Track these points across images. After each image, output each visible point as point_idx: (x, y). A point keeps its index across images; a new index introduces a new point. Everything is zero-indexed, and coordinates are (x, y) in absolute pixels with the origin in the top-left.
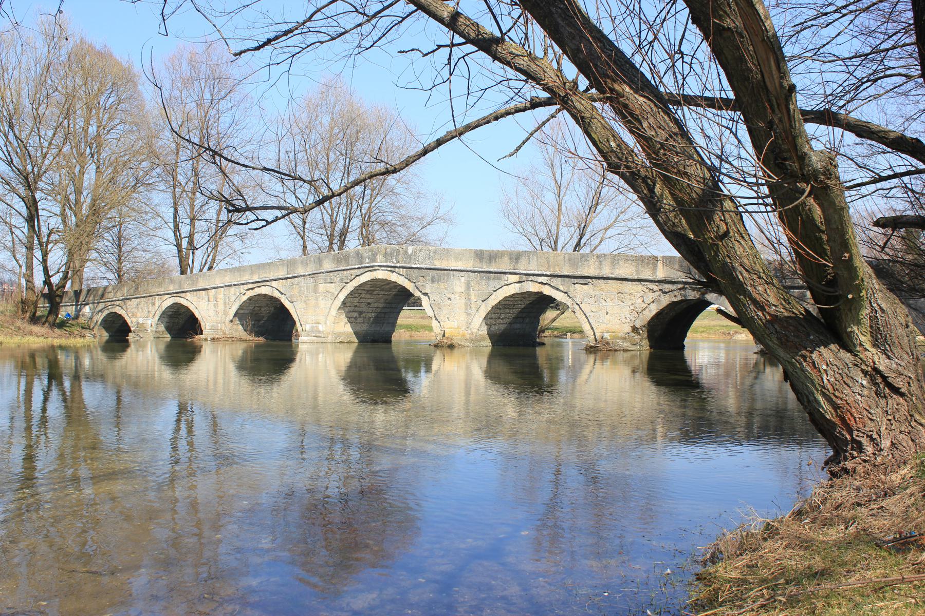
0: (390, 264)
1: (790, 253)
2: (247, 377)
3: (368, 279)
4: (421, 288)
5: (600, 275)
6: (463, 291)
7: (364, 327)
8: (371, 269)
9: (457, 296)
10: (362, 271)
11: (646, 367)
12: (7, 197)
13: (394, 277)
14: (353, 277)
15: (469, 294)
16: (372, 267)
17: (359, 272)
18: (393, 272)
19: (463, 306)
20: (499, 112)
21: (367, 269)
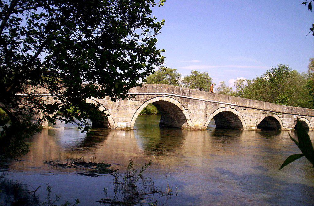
0: (170, 94)
1: (101, 129)
2: (139, 132)
3: (158, 100)
4: (185, 107)
5: (250, 107)
6: (204, 109)
7: (106, 131)
8: (160, 96)
9: (201, 111)
10: (155, 96)
11: (309, 161)
12: (286, 137)
13: (171, 100)
14: (150, 98)
15: (206, 111)
16: (162, 94)
17: (155, 96)
18: (170, 98)
19: (204, 116)
20: (198, 127)
21: (158, 95)
